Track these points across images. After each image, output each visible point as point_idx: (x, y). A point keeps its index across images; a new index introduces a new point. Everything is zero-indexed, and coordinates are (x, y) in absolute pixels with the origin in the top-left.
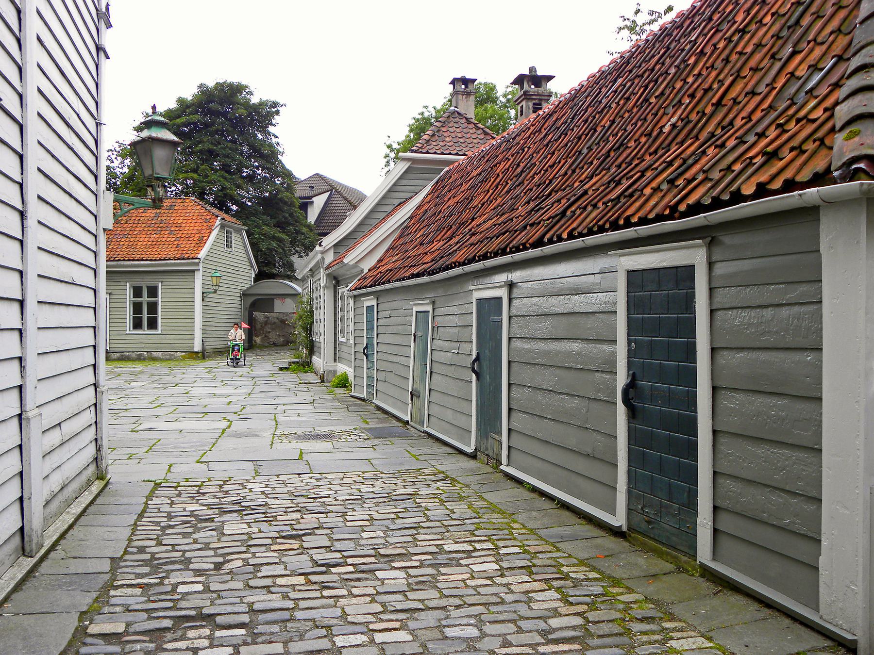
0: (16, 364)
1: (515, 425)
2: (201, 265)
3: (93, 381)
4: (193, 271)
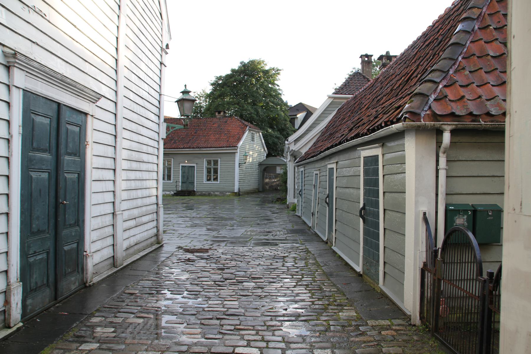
0: (112, 193)
1: (338, 228)
2: (238, 150)
3: (156, 202)
4: (235, 153)
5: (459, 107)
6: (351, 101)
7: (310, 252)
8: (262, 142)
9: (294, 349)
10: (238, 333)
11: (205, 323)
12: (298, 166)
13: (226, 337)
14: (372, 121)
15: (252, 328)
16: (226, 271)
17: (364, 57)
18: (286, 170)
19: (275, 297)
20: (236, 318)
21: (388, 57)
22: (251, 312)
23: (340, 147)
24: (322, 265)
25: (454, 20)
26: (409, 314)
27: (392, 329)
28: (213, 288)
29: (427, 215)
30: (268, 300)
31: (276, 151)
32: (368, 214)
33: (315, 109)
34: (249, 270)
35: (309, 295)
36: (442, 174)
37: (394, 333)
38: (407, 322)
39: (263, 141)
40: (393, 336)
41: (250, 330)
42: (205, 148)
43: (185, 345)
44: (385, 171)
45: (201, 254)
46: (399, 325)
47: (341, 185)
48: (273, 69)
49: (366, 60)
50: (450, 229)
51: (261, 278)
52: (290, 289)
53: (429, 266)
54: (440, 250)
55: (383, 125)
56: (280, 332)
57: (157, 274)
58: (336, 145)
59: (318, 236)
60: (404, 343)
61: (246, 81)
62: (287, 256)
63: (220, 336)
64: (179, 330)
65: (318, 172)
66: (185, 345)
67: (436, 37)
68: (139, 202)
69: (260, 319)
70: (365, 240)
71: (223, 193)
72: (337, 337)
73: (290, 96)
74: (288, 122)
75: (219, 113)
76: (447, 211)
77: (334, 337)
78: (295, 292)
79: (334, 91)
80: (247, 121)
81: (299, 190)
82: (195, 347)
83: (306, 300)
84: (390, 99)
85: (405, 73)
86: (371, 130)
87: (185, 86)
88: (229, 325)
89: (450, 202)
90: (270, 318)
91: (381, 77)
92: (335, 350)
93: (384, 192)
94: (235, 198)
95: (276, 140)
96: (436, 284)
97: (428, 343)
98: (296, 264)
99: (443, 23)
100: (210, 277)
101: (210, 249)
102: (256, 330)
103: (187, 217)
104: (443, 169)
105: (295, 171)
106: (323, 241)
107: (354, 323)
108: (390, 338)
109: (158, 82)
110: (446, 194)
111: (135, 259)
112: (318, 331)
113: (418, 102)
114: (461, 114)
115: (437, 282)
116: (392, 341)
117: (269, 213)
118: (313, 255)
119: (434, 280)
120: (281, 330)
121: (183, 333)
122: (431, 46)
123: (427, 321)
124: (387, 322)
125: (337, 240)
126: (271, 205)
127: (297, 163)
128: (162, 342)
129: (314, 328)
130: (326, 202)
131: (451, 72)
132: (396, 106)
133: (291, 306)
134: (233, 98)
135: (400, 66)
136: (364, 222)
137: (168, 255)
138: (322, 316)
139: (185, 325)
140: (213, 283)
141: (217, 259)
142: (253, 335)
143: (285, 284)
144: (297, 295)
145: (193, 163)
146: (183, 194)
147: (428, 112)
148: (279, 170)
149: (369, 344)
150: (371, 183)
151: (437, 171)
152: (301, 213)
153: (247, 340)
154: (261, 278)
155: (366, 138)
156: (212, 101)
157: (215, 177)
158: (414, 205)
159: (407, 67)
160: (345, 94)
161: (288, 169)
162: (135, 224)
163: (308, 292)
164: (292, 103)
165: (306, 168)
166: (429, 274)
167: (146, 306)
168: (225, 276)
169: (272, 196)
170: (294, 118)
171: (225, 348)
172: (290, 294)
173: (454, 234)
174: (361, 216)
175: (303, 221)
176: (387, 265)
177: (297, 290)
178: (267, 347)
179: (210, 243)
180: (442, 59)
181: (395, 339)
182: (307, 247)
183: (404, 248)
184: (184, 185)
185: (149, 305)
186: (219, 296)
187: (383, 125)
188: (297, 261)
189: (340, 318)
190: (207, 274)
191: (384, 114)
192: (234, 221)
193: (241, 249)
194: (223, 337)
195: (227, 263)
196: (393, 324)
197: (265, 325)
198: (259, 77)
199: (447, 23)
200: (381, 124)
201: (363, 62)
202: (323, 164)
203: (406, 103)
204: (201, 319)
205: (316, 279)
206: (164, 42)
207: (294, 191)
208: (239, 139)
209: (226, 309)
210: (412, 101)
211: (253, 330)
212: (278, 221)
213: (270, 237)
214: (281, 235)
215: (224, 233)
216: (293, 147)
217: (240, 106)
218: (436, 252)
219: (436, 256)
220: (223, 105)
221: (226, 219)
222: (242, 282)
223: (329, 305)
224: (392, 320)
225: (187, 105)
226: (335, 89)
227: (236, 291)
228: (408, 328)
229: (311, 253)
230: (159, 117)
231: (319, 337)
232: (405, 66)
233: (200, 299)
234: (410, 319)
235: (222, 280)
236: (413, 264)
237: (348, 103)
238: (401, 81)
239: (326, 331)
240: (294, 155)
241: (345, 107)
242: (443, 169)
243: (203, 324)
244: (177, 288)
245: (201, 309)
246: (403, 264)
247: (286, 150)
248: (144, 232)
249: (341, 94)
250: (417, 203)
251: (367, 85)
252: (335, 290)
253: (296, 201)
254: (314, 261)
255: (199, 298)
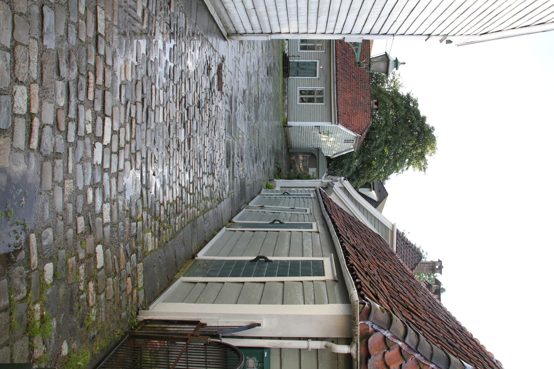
1: (246, 233)
2: (335, 125)
3: (274, 32)
4: (331, 121)
5: (377, 363)
6: (389, 249)
7: (219, 202)
8: (343, 152)
9: (110, 182)
10: (127, 121)
11: (138, 85)
12: (316, 191)
13: (123, 108)
14: (363, 269)
15: (133, 137)
16: (197, 110)
17: (439, 265)
18: (312, 179)
19: (168, 163)
20: (144, 120)
21: (438, 291)
22: (151, 136)
23: (334, 235)
24: (205, 215)
25: (478, 361)
26: (151, 308)
27: (133, 289)
28: (178, 95)
29: (257, 327)
30: (164, 155)
31: (334, 168)
32: (260, 265)
33: (381, 211)
34: (198, 135)
35: (171, 201)
36: (303, 344)
37: (129, 291)
38: (141, 306)
39: (345, 153)
40: (126, 290)
41: (131, 135)
42: (337, 88)
43: (113, 63)
44: (307, 282)
45: (216, 83)
46: (138, 296)
47: (293, 236)
48: (426, 164)
49: (435, 267)
50: (242, 352)
51: (189, 149)
52: (178, 180)
53: (202, 329)
54: (219, 341)
55: (357, 280)
56: (130, 168)
57: (193, 34)
58: (337, 231)
59: (238, 213)
60: (118, 301)
61: (412, 134)
62: (214, 178)
63: (123, 101)
64: (130, 57)
65: (308, 212)
66: (113, 63)
67: (458, 341)
68: (273, 13)
69: (143, 145)
70: (232, 262)
71: (286, 108)
72: (124, 229)
73: (394, 183)
74: (366, 181)
75: (376, 104)
76: (262, 349)
77: (124, 225)
78: (174, 185)
79: (401, 231)
80: (368, 134)
81: (289, 192)
82: (110, 74)
83: (165, 197)
84: (387, 289)
85: (418, 306)
86: (352, 268)
87: (404, 63)
88: (136, 111)
89: (272, 352)
90: (145, 157)
91: (414, 282)
92: (109, 226)
93: (283, 282)
94: (281, 121)
95: (346, 167)
96: (182, 337)
97: (118, 328)
98: (206, 187)
99: (475, 350)
100: (190, 92)
101: (222, 93)
102: (131, 141)
103: (259, 68)
104: (308, 345)
105: (310, 187)
106: (232, 218)
107: (140, 248)
108: (123, 286)
109: (408, 33)
110: (281, 349)
111: (210, 9)
112: (130, 209)
113: (381, 318)
114: (369, 365)
115: (184, 337)
116: (120, 288)
117: (263, 159)
118: (217, 207)
119: (187, 334)
120: (131, 169)
121: (126, 61)
122: (448, 336)
123: (142, 327)
124: (141, 284)
125: (233, 232)
126: (273, 161)
127: (320, 189)
128: (116, 37)
129: (133, 204)
130: (275, 221)
131: (417, 356)
132: (379, 295)
133: (158, 180)
134: (392, 118)
135: (426, 302)
136: (251, 261)
137: (214, 46)
138: (148, 213)
139: (136, 63)
140: (183, 95)
141: (211, 100)
142: (125, 138)
143: (183, 175)
144: (171, 188)
145: (320, 75)
146: (285, 64)
147: (370, 329)
148: (312, 171)
149: (116, 263)
150: (294, 269)
151: (306, 339)
152: (263, 195)
153: (119, 130)
154: (189, 149)
155: (343, 263)
156: (389, 96)
157: (305, 100)
158: (268, 313)
159: (424, 309)
160: (397, 243)
161: (313, 180)
162: (249, 8)
163: (175, 199)
164: (388, 185)
165: (313, 199)
166: (193, 329)
167: (156, 20)
168: (192, 109)
169: (283, 163)
170: (370, 187)
171: (110, 107)
172: (171, 180)
173: (236, 355)
174: (258, 258)
175: (255, 197)
176: (203, 285)
177: (177, 188)
178: (112, 153)
179: (229, 93)
180: (431, 346)
181: (123, 292)
182: (225, 200)
183: (222, 303)
184: (295, 65)
185: (157, 24)
186: (168, 101)
187: (357, 280)
188: (209, 188)
189: (144, 233)
190: (193, 89)
191: (370, 282)
192: (254, 121)
193: (222, 127)
194: (122, 104)
195: (206, 112)
196: (138, 290)
197: (137, 151)
198: (417, 148)
199: (475, 353)
200: (359, 278)
201: (433, 264)
202: (318, 218)
203: (381, 306)
204: (143, 82)
205: (189, 209)
206: (454, 37)
207: (288, 187)
208: (346, 126)
209: (153, 108)
210: (383, 312)
211: (131, 137)
212: (255, 168)
213: (237, 160)
214: (239, 171)
215: (241, 108)
216: (337, 186)
217: (384, 127)
218: (217, 337)
219: (213, 336)
220: (385, 107)
221: (256, 111)
222: (184, 127)
223: (160, 221)
224: (143, 290)
225: (382, 65)
226: (403, 233)
227: (174, 121)
228: (135, 308)
229: (219, 203)
230: (369, 34)
231: (124, 210)
232: (426, 307)
233: (164, 81)
234: (144, 309)
235: (187, 105)
236: (204, 312)
237: (387, 246)
238: (408, 302)
239: (131, 218)
240: (328, 187)
241: (381, 242)
242: (308, 345)
243: (137, 83)
244: (177, 55)
245: (153, 81)
246: (204, 302)
247: (334, 178)
248: (239, 19)
249: (397, 239)
250: (271, 316)
251: (408, 269)
252: (177, 229)
253: (278, 188)
254: (209, 207)
255: (167, 79)
